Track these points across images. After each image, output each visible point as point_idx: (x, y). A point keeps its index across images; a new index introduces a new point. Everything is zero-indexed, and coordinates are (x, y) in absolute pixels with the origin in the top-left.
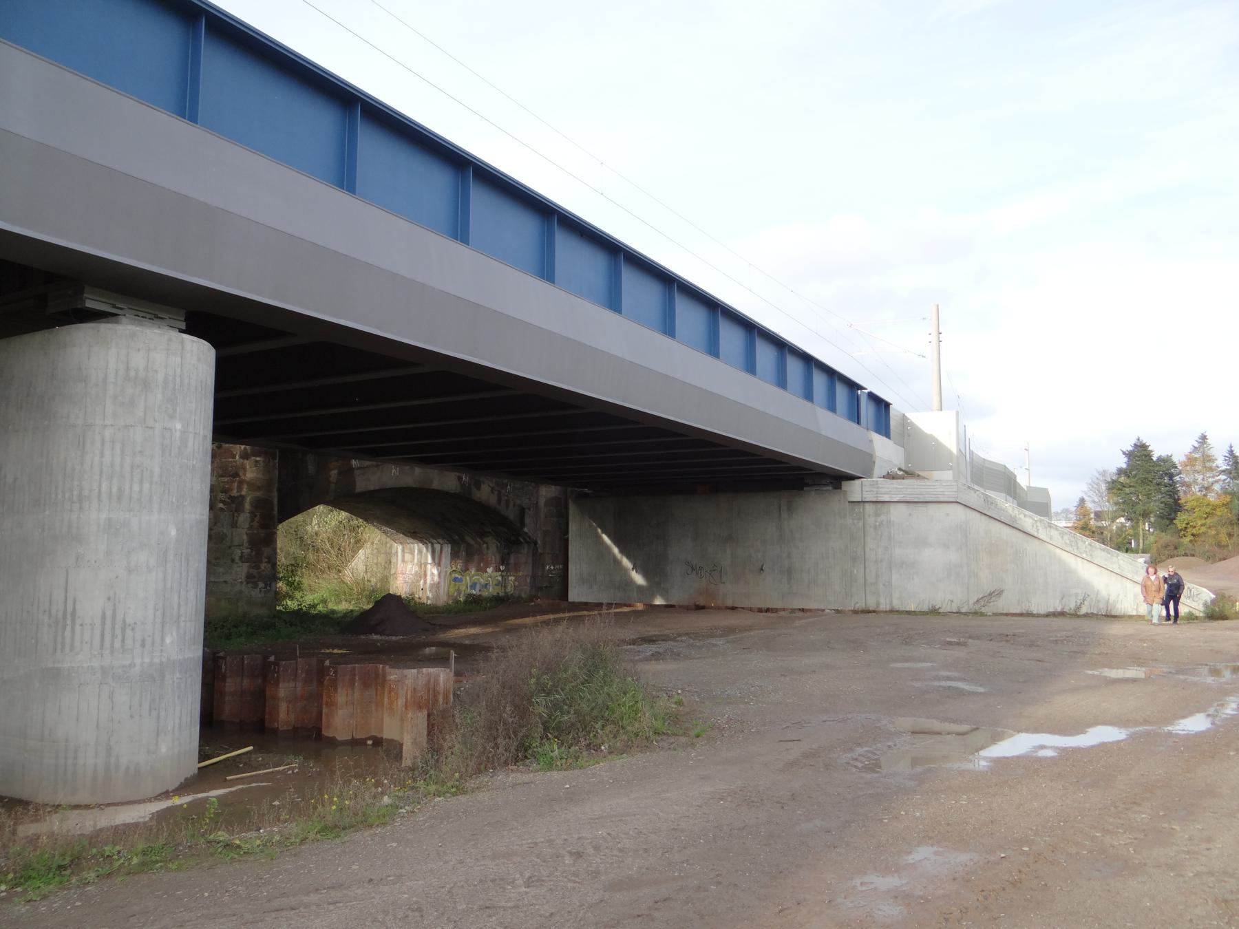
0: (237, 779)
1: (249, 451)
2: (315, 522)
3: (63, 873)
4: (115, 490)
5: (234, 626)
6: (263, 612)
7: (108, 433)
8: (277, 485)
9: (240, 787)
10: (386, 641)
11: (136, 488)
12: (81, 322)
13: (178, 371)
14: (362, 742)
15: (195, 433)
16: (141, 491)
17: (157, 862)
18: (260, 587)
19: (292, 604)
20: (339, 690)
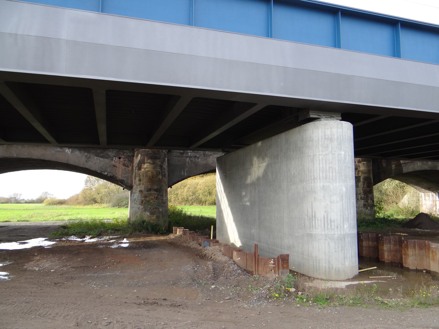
0: (373, 278)
1: (361, 160)
2: (386, 185)
3: (327, 301)
4: (324, 176)
5: (361, 223)
6: (370, 218)
7: (321, 157)
8: (372, 172)
9: (375, 281)
10: (423, 231)
11: (331, 175)
12: (309, 122)
13: (341, 134)
14: (421, 271)
15: (349, 155)
16: (332, 176)
17: (358, 304)
18: (369, 209)
19: (381, 215)
20: (409, 250)
